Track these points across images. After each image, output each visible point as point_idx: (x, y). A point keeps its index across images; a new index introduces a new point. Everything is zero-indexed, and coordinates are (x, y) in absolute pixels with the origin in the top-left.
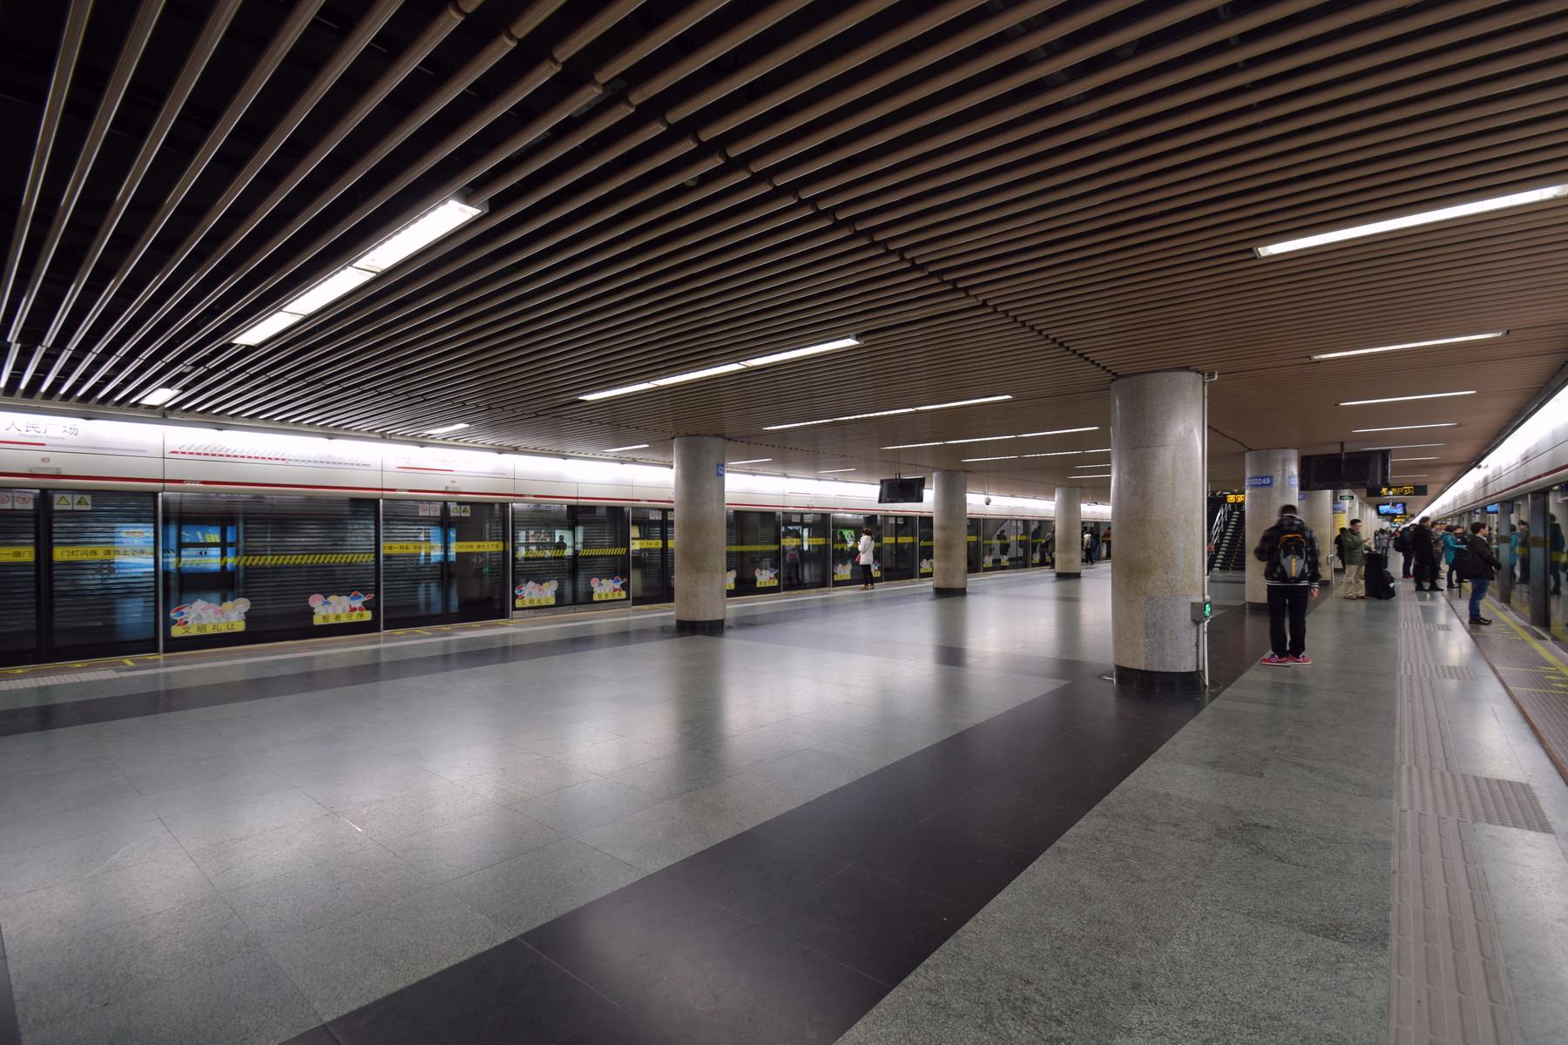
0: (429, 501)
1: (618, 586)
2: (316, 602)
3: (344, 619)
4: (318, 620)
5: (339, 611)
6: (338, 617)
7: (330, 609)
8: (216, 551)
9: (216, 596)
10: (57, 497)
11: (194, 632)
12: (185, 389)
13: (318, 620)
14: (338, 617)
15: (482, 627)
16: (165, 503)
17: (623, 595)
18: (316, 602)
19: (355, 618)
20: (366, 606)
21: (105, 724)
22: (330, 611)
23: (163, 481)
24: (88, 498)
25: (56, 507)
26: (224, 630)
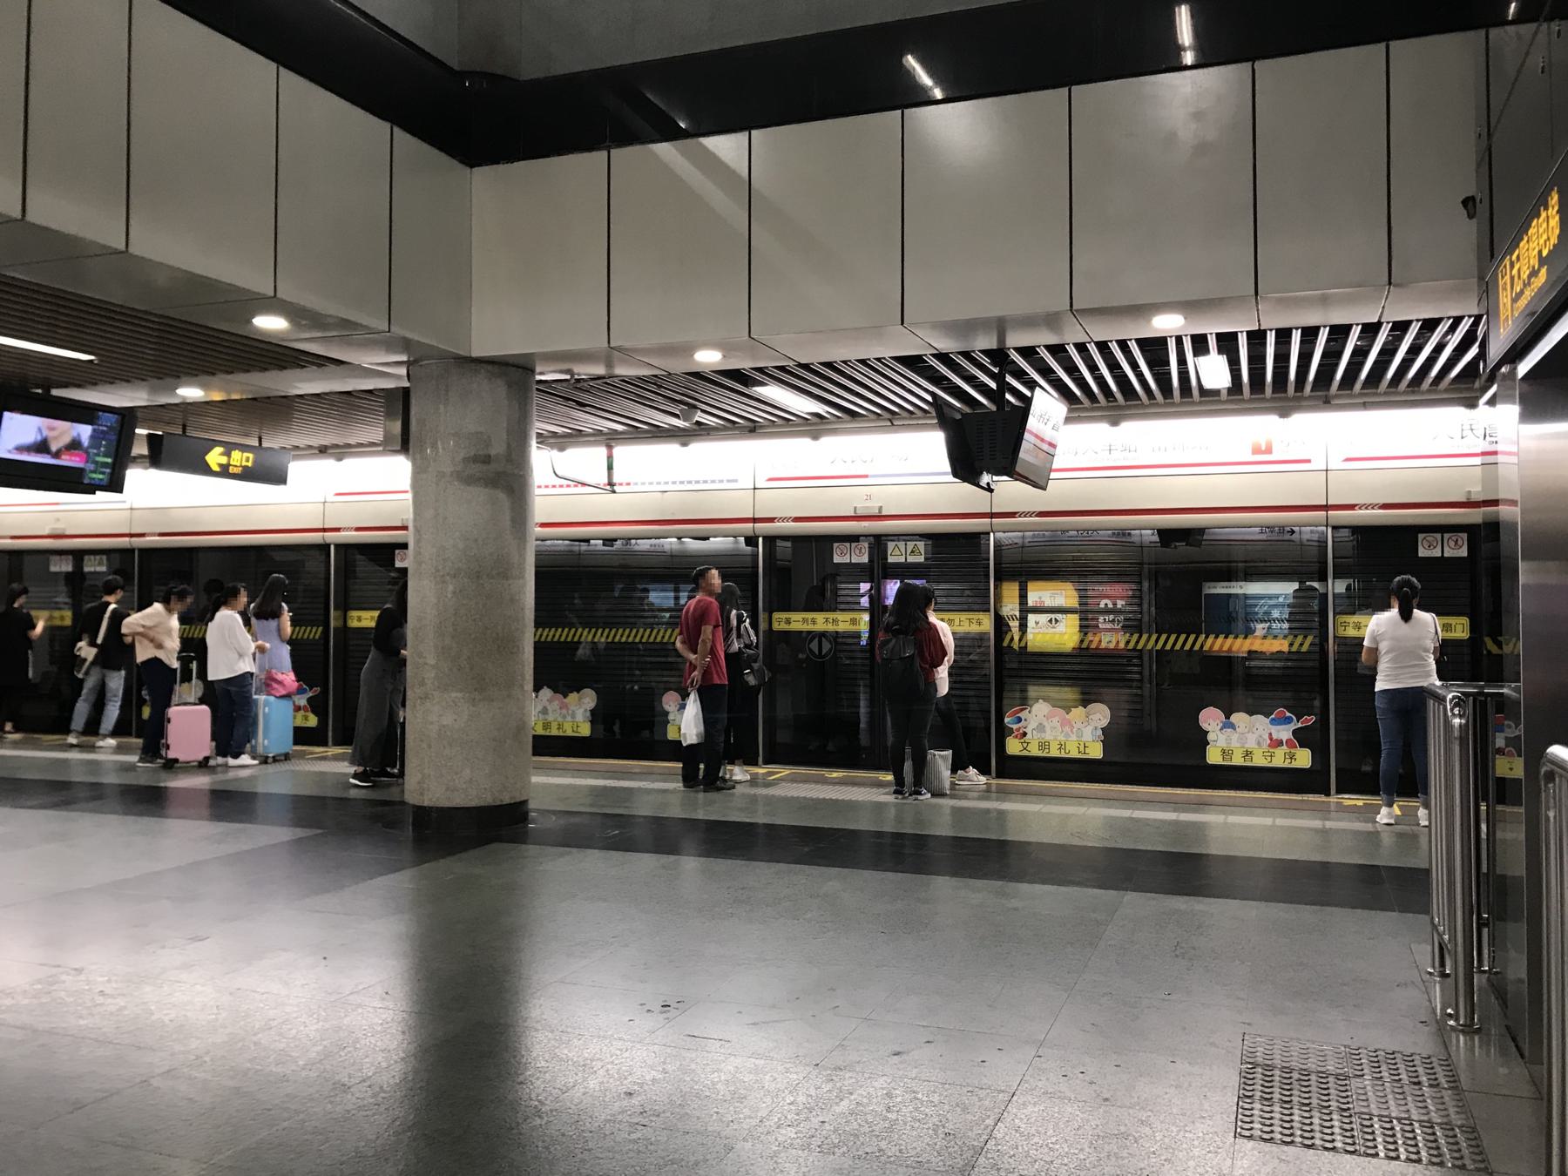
0: (853, 538)
1: (1285, 733)
2: (1210, 719)
3: (1259, 761)
4: (1214, 757)
5: (1251, 744)
6: (1248, 754)
7: (1241, 737)
8: (1074, 620)
9: (1069, 693)
10: (891, 545)
11: (1034, 751)
12: (1032, 385)
13: (1214, 757)
14: (1248, 754)
15: (564, 770)
16: (998, 546)
17: (1303, 759)
18: (1210, 719)
19: (1279, 760)
20: (1302, 738)
21: (1212, 900)
22: (1235, 744)
23: (992, 515)
24: (921, 545)
25: (891, 560)
26: (1074, 754)
